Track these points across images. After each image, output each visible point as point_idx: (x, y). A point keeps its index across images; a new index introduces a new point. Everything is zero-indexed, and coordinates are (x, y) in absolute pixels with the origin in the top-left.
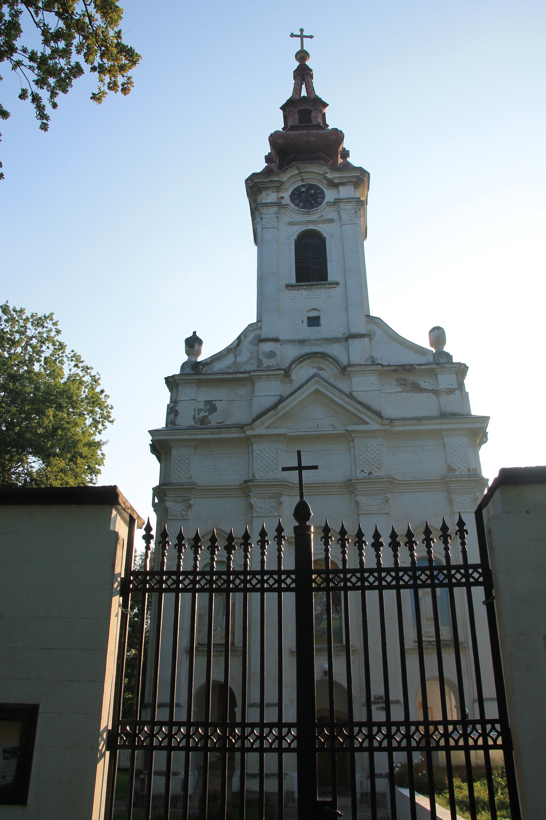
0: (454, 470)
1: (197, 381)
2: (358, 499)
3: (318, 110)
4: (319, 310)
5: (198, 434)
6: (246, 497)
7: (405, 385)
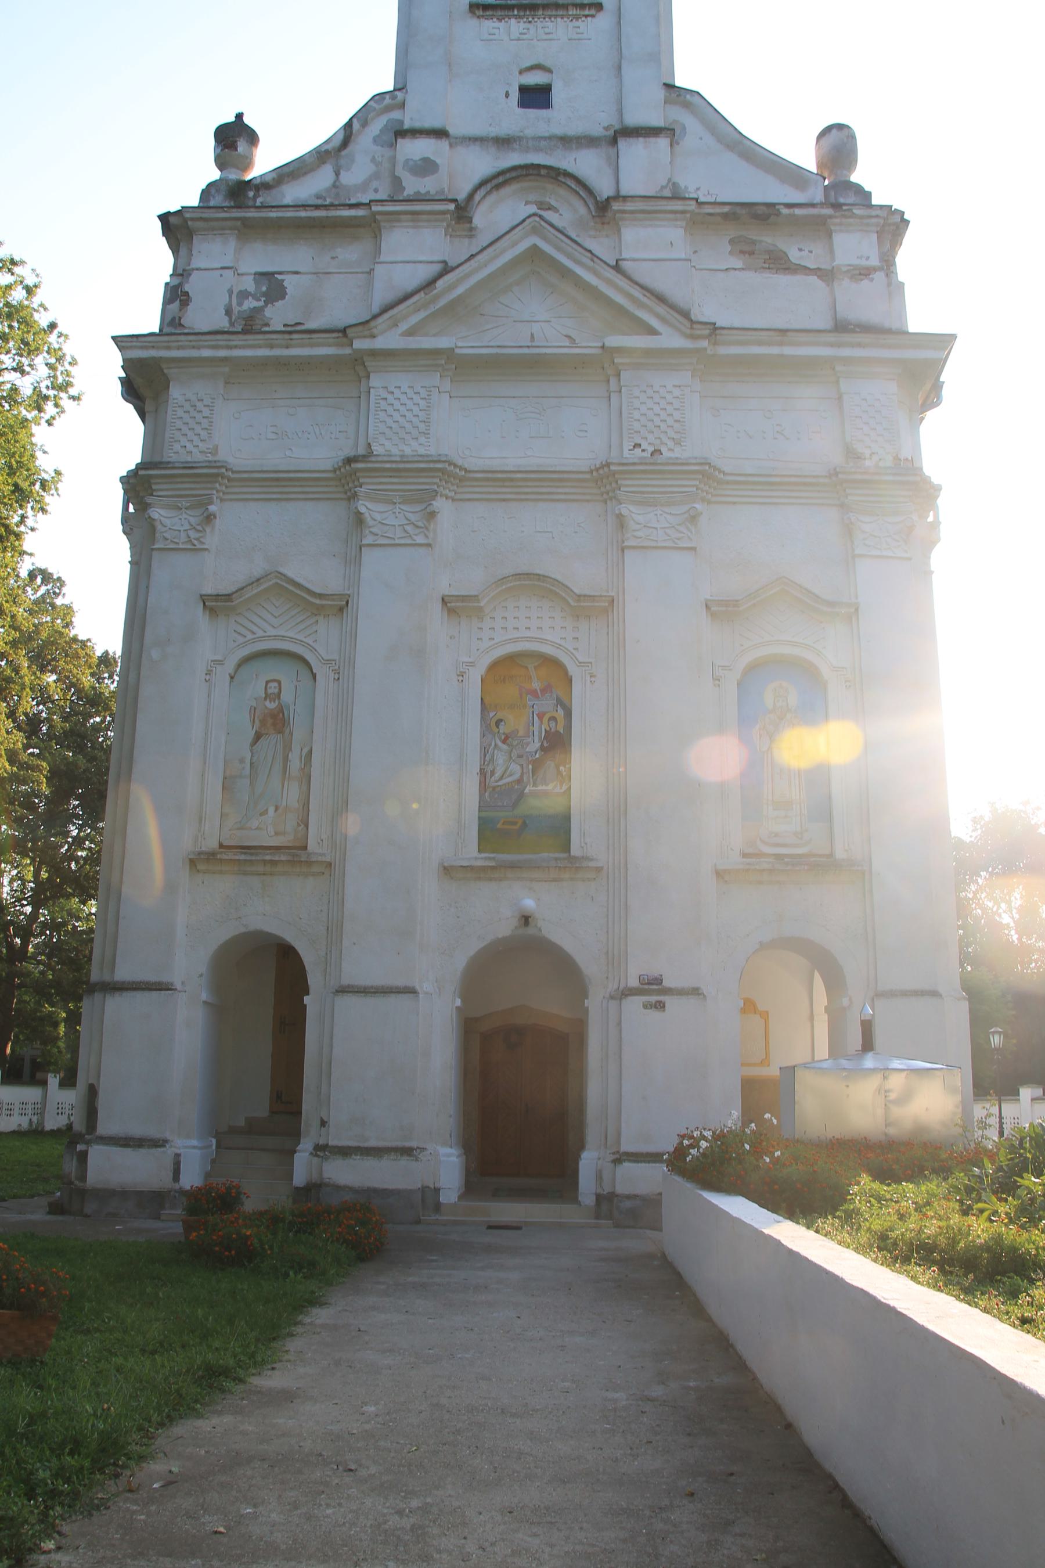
0: (859, 458)
1: (239, 223)
2: (624, 512)
4: (549, 71)
5: (236, 347)
6: (349, 499)
7: (751, 253)
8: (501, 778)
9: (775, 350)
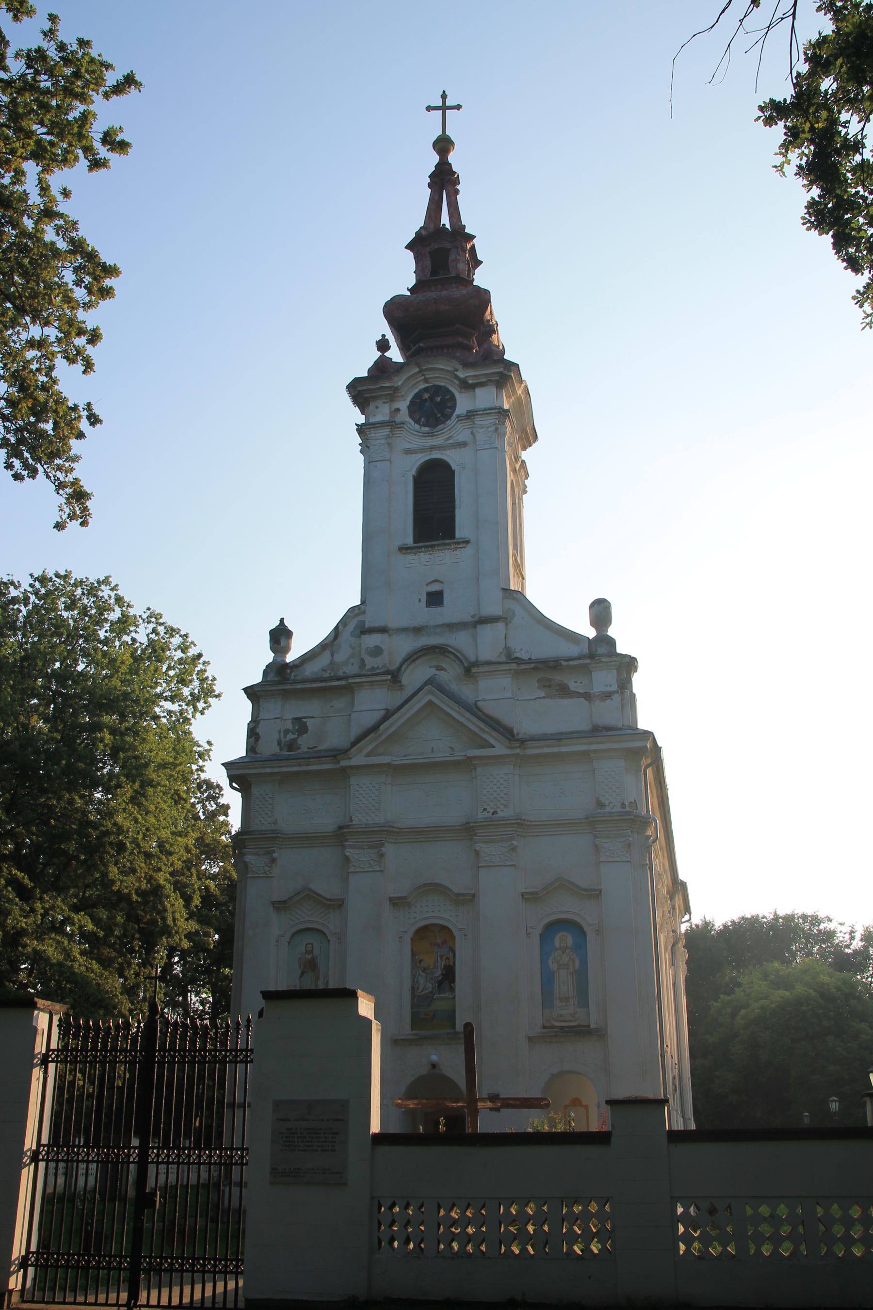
3: (458, 248)
5: (283, 766)
7: (549, 686)
8: (422, 991)
9: (556, 750)
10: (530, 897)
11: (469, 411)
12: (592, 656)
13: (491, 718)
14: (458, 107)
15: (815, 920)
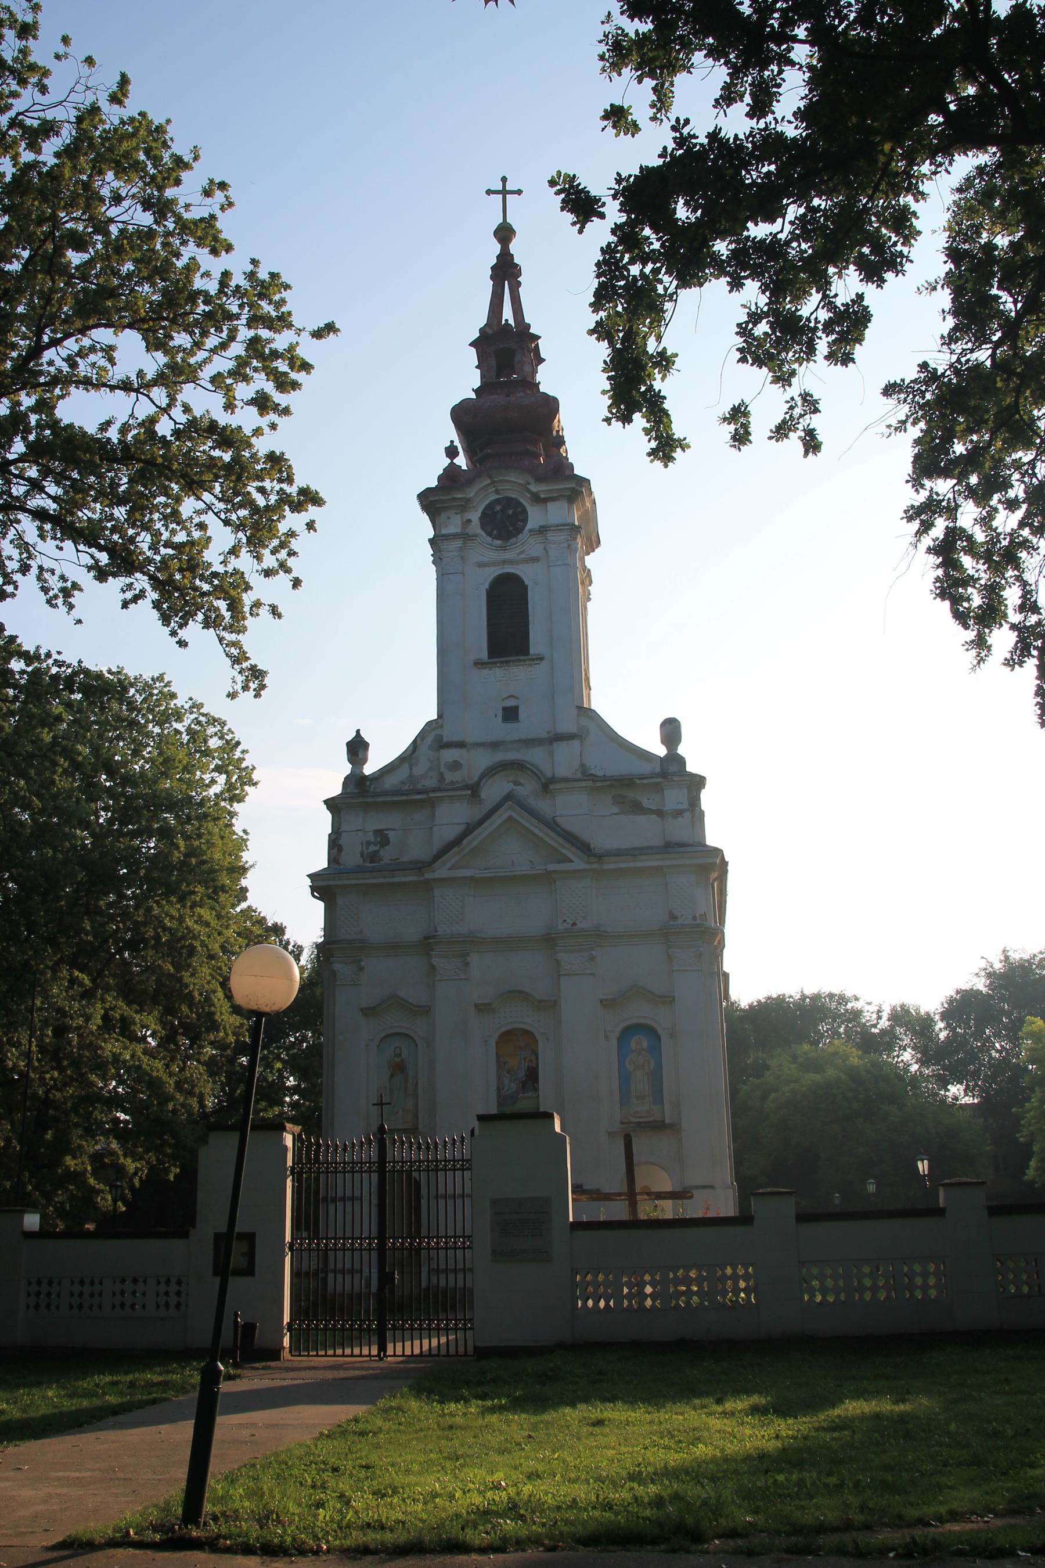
7: (623, 803)
10: (608, 1004)
11: (541, 527)
12: (664, 774)
13: (568, 833)
14: (519, 192)
15: (842, 999)
